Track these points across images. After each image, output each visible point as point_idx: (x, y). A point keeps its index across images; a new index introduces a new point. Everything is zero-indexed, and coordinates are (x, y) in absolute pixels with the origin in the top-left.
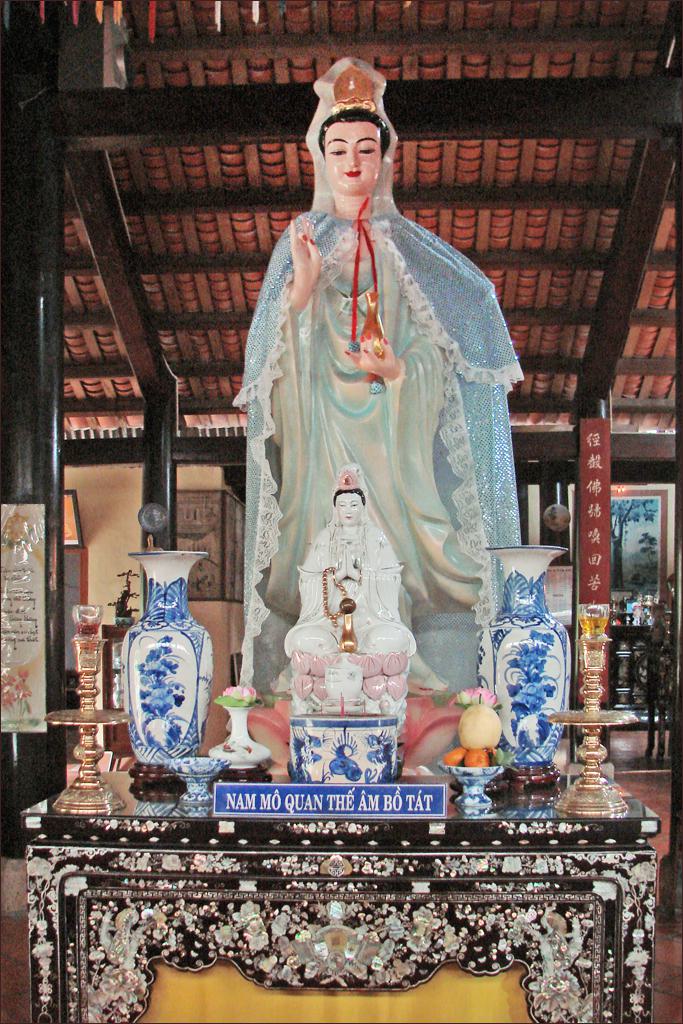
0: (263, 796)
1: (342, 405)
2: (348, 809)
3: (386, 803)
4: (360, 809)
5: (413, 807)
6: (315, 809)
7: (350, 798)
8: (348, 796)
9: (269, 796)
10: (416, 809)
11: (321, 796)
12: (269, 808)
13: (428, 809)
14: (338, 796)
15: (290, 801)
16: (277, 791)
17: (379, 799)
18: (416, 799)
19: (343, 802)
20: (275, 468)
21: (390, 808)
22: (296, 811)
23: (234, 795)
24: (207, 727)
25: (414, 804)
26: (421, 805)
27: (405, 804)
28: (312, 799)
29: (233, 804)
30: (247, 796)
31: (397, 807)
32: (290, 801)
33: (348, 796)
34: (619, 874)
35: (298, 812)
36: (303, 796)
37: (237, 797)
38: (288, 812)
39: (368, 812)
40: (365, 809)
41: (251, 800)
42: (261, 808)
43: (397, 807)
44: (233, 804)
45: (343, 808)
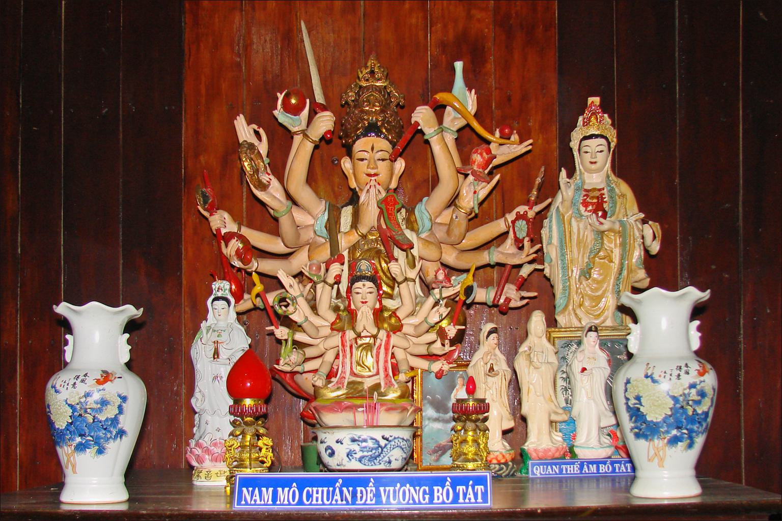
0: (280, 489)
1: (386, 271)
2: (575, 472)
3: (436, 494)
4: (583, 472)
5: (464, 498)
6: (554, 473)
7: (371, 491)
8: (575, 466)
9: (286, 489)
10: (621, 471)
11: (351, 489)
12: (286, 502)
13: (629, 470)
14: (315, 489)
15: (537, 469)
16: (294, 484)
17: (273, 491)
18: (467, 489)
19: (320, 495)
20: (274, 257)
21: (441, 500)
22: (541, 474)
23: (250, 489)
24: (152, 406)
25: (465, 495)
26: (472, 496)
27: (456, 496)
28: (552, 468)
29: (249, 498)
30: (264, 489)
31: (448, 499)
32: (537, 469)
33: (575, 466)
34: (333, 379)
35: (543, 475)
36: (331, 489)
37: (253, 492)
38: (537, 475)
39: (589, 473)
40: (587, 472)
41: (268, 493)
42: (278, 502)
43: (448, 499)
44: (249, 498)
45: (572, 472)
